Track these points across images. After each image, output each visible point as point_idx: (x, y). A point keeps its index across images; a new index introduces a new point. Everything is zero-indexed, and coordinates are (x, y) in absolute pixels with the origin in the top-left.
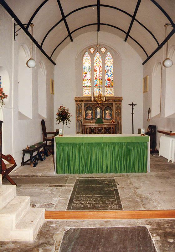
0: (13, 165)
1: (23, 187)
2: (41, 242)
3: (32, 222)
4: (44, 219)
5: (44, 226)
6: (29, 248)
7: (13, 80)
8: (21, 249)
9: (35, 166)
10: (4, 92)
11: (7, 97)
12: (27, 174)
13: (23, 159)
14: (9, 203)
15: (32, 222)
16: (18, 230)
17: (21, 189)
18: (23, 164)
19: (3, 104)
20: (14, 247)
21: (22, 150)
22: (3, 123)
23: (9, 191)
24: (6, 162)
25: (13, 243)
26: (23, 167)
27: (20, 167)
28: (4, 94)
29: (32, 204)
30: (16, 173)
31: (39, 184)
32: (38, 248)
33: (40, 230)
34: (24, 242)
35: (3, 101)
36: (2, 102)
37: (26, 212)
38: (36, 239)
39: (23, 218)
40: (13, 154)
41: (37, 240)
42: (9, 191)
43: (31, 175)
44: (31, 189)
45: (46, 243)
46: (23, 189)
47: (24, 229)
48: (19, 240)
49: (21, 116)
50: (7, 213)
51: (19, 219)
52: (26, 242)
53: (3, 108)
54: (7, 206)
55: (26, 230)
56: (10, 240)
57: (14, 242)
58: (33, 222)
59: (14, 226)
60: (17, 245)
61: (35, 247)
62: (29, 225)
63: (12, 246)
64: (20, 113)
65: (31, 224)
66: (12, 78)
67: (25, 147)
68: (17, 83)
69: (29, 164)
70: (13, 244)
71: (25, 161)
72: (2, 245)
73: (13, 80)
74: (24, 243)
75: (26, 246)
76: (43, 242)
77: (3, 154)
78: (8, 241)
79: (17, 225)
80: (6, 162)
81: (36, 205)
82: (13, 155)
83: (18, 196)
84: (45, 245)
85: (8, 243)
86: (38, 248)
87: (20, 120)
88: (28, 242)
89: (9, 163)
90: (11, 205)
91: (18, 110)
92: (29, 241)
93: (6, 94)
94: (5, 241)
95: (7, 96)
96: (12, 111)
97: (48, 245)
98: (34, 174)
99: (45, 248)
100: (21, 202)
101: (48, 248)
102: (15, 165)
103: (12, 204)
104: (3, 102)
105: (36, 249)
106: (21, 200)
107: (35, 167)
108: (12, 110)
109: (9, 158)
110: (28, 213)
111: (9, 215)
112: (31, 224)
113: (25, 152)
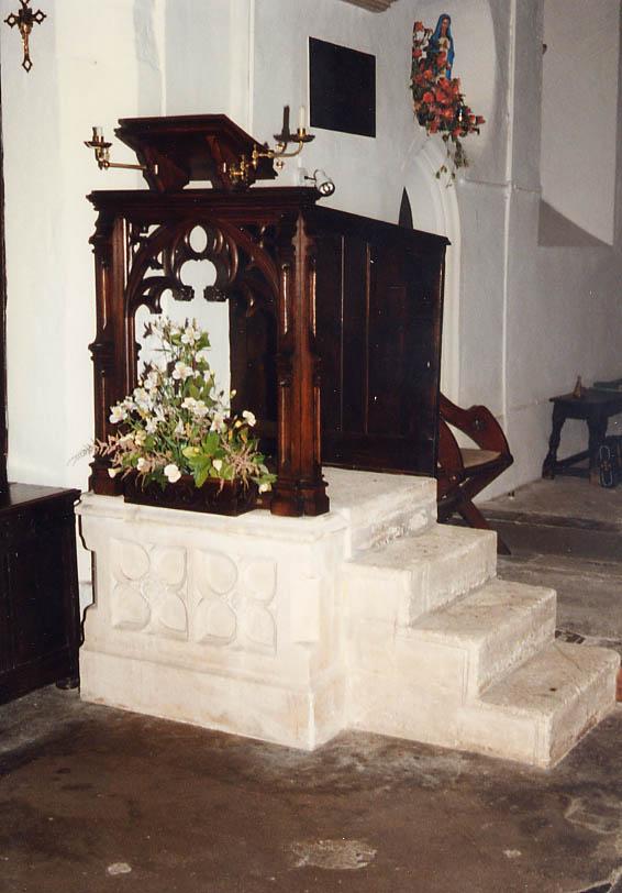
0: (495, 455)
1: (538, 563)
2: (581, 776)
3: (553, 690)
4: (614, 698)
5: (610, 726)
6: (528, 786)
7: (512, 33)
8: (496, 784)
9: (613, 486)
10: (466, 102)
11: (480, 126)
12: (565, 516)
13: (554, 442)
14: (460, 598)
15: (553, 690)
16: (488, 706)
17: (529, 569)
18: (552, 467)
19: (458, 164)
20: (467, 771)
21: (551, 400)
22: (448, 247)
23: (465, 550)
24: (463, 440)
25: (463, 758)
26: (550, 484)
27: (537, 482)
28: (466, 110)
29: (568, 633)
30: (512, 504)
31: (614, 563)
32: (567, 795)
33: (588, 735)
34: (509, 763)
35: (459, 145)
36: (454, 150)
37: (532, 653)
38: (562, 762)
39: (518, 669)
40: (504, 413)
41: (569, 768)
42: (465, 550)
43: (585, 521)
44: (573, 574)
45: (604, 788)
46: (537, 570)
47: (515, 709)
48: (490, 749)
49: (552, 227)
50: (447, 629)
51: (496, 664)
52: (518, 764)
53: (462, 181)
54: (450, 607)
55: (523, 712)
56: (455, 745)
57: (473, 757)
58: (558, 691)
59: (474, 689)
60: (480, 767)
61: (556, 788)
62: (540, 698)
63: (461, 766)
64: (545, 210)
65: (545, 696)
66: (506, 28)
67: (566, 387)
68: (533, 50)
69: (581, 473)
70: (465, 762)
71: (561, 455)
72: (419, 753)
73: (512, 33)
74: (511, 768)
75: (517, 778)
76: (594, 780)
77: (457, 404)
78: (447, 745)
79: (458, 609)
80: (463, 440)
81: (586, 637)
82: (501, 417)
83: (505, 582)
84: (600, 791)
85: (447, 752)
86: (567, 795)
87: (543, 249)
88: (527, 767)
89: (478, 448)
90: (470, 607)
91: (539, 189)
92: (531, 763)
93: (475, 112)
94: (434, 743)
95: (479, 120)
96: (503, 198)
97: (613, 796)
98: (599, 518)
99: (597, 801)
100: (511, 605)
101: (609, 805)
102: (506, 460)
103: (469, 603)
104: (458, 154)
105: (557, 798)
106: (513, 597)
107: (613, 492)
108: (508, 192)
109: (480, 422)
110: (540, 655)
111: (456, 638)
112: (545, 696)
113: (564, 408)
